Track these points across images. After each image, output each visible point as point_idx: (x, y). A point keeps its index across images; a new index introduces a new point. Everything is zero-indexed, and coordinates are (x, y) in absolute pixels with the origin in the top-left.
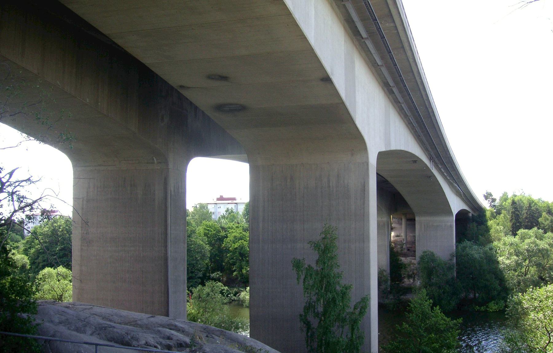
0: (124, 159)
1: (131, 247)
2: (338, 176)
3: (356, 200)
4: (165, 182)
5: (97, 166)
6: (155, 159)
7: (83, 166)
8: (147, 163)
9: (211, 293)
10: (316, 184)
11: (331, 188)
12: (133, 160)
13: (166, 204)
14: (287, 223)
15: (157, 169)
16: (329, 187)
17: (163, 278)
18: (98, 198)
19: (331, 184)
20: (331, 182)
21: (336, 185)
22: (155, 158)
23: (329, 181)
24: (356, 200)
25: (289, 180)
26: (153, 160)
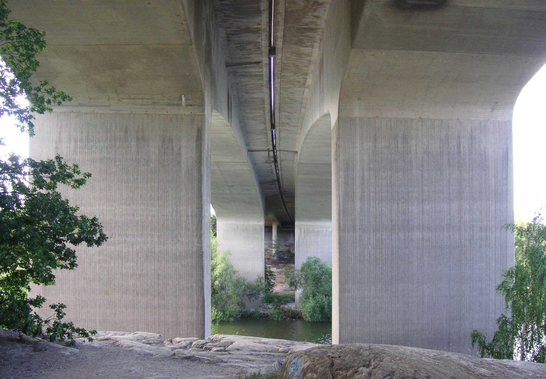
0: (129, 96)
1: (138, 236)
2: (471, 138)
3: (496, 173)
4: (198, 137)
5: (77, 106)
6: (183, 99)
7: (255, 98)
8: (169, 105)
9: (165, 129)
10: (440, 148)
11: (462, 155)
12: (423, 200)
13: (201, 170)
14: (397, 203)
15: (185, 115)
16: (459, 153)
17: (194, 285)
18: (77, 158)
19: (462, 149)
20: (462, 147)
21: (469, 150)
22: (184, 97)
23: (459, 145)
24: (496, 173)
25: (400, 141)
26: (180, 99)
